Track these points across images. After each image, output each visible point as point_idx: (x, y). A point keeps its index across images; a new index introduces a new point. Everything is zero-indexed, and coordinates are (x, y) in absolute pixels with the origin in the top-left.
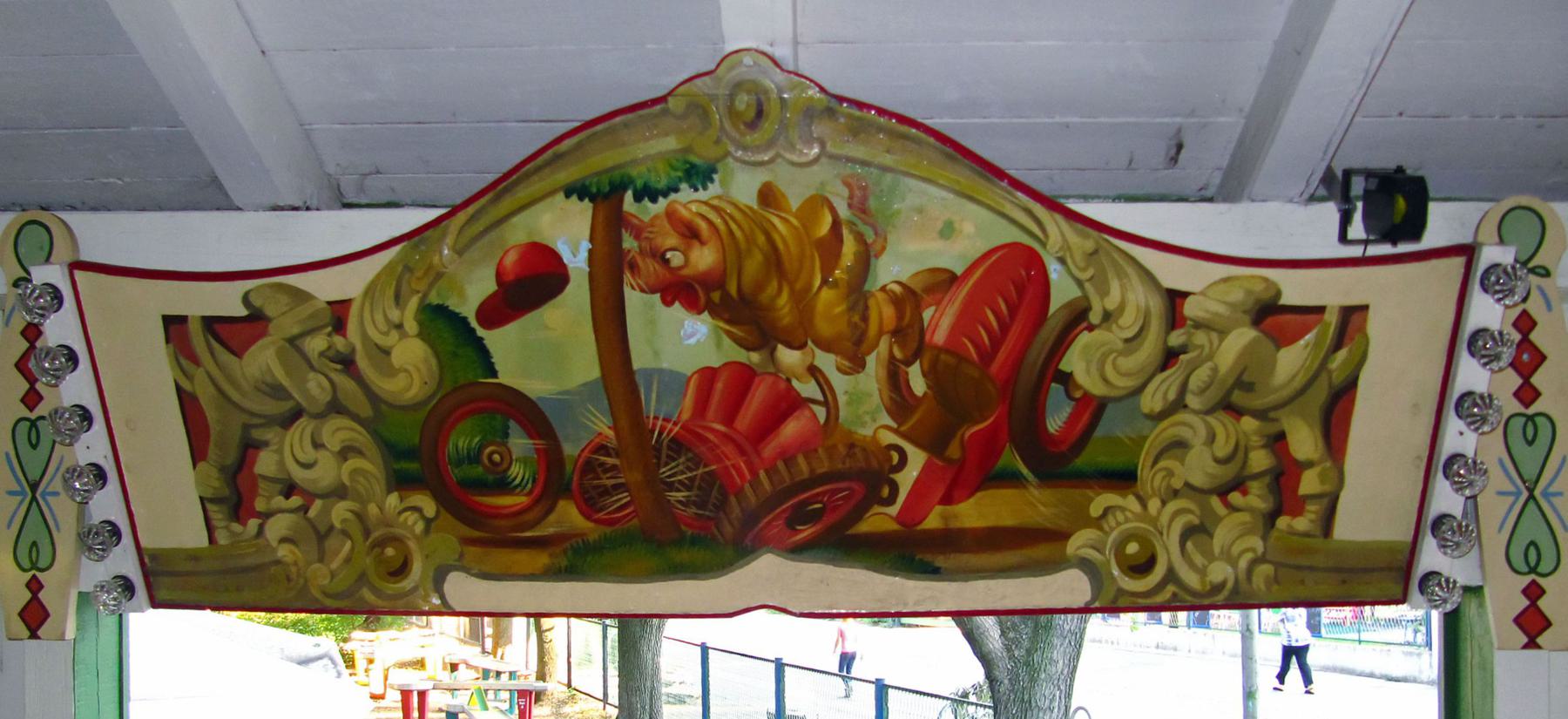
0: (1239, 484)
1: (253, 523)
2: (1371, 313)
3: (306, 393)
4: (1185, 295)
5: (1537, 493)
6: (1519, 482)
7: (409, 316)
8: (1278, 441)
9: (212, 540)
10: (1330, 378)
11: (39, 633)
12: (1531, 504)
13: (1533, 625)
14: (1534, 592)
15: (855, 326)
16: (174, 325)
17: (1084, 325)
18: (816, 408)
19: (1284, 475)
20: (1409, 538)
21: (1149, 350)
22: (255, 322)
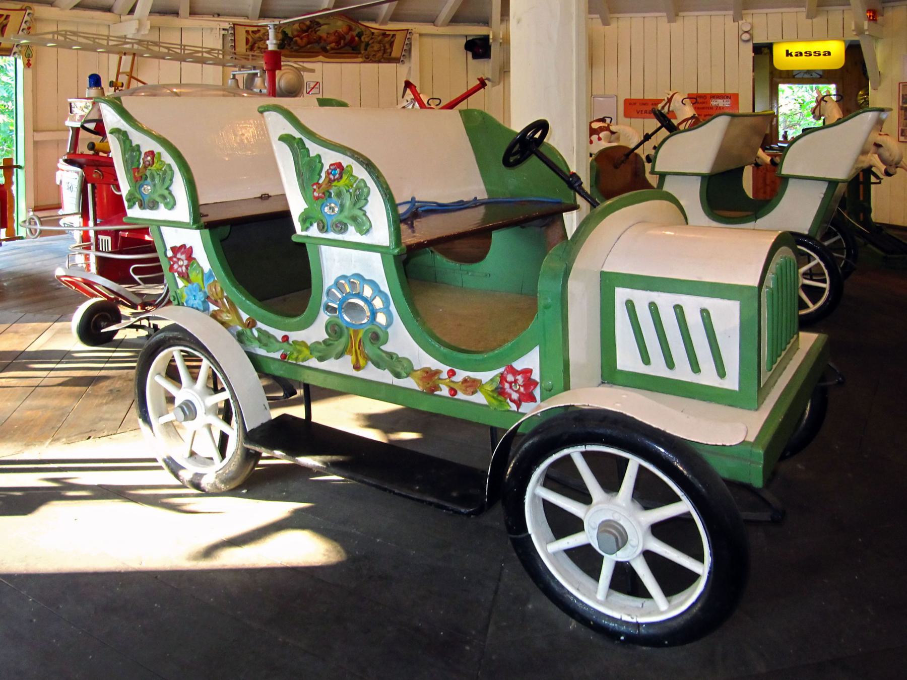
0: (380, 50)
8: (385, 47)
15: (288, 26)
16: (247, 32)
17: (468, 39)
18: (832, 97)
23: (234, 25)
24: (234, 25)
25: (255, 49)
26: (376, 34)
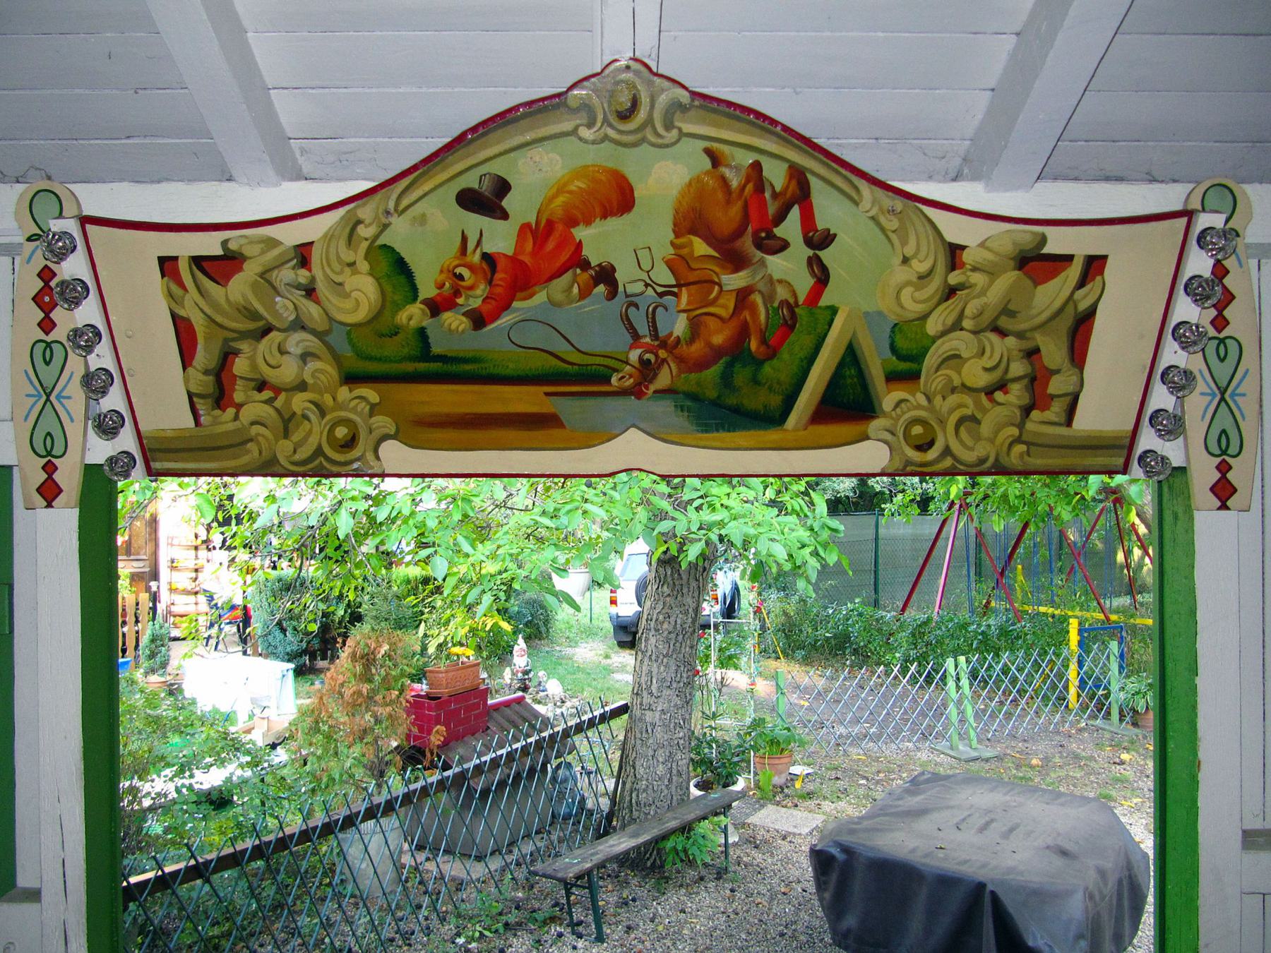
0: (1002, 386)
1: (231, 411)
2: (1109, 261)
3: (276, 314)
4: (963, 248)
5: (1227, 396)
6: (1213, 385)
7: (359, 256)
8: (1032, 354)
9: (197, 423)
10: (1076, 307)
11: (53, 504)
12: (1223, 404)
13: (1224, 491)
14: (1224, 468)
16: (167, 265)
19: (1037, 380)
20: (1131, 427)
21: (935, 285)
25: (238, 397)
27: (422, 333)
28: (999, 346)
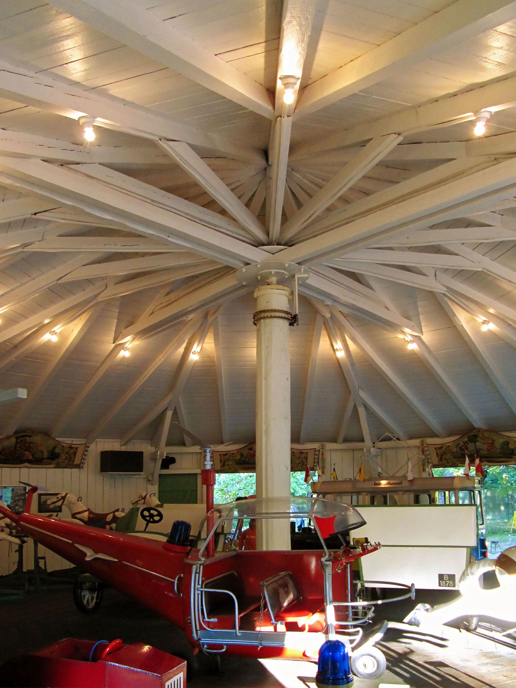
2: (78, 448)
8: (70, 456)
21: (61, 450)
22: (442, 447)
23: (213, 451)
24: (213, 451)
26: (295, 452)
27: (244, 460)
28: (66, 455)
